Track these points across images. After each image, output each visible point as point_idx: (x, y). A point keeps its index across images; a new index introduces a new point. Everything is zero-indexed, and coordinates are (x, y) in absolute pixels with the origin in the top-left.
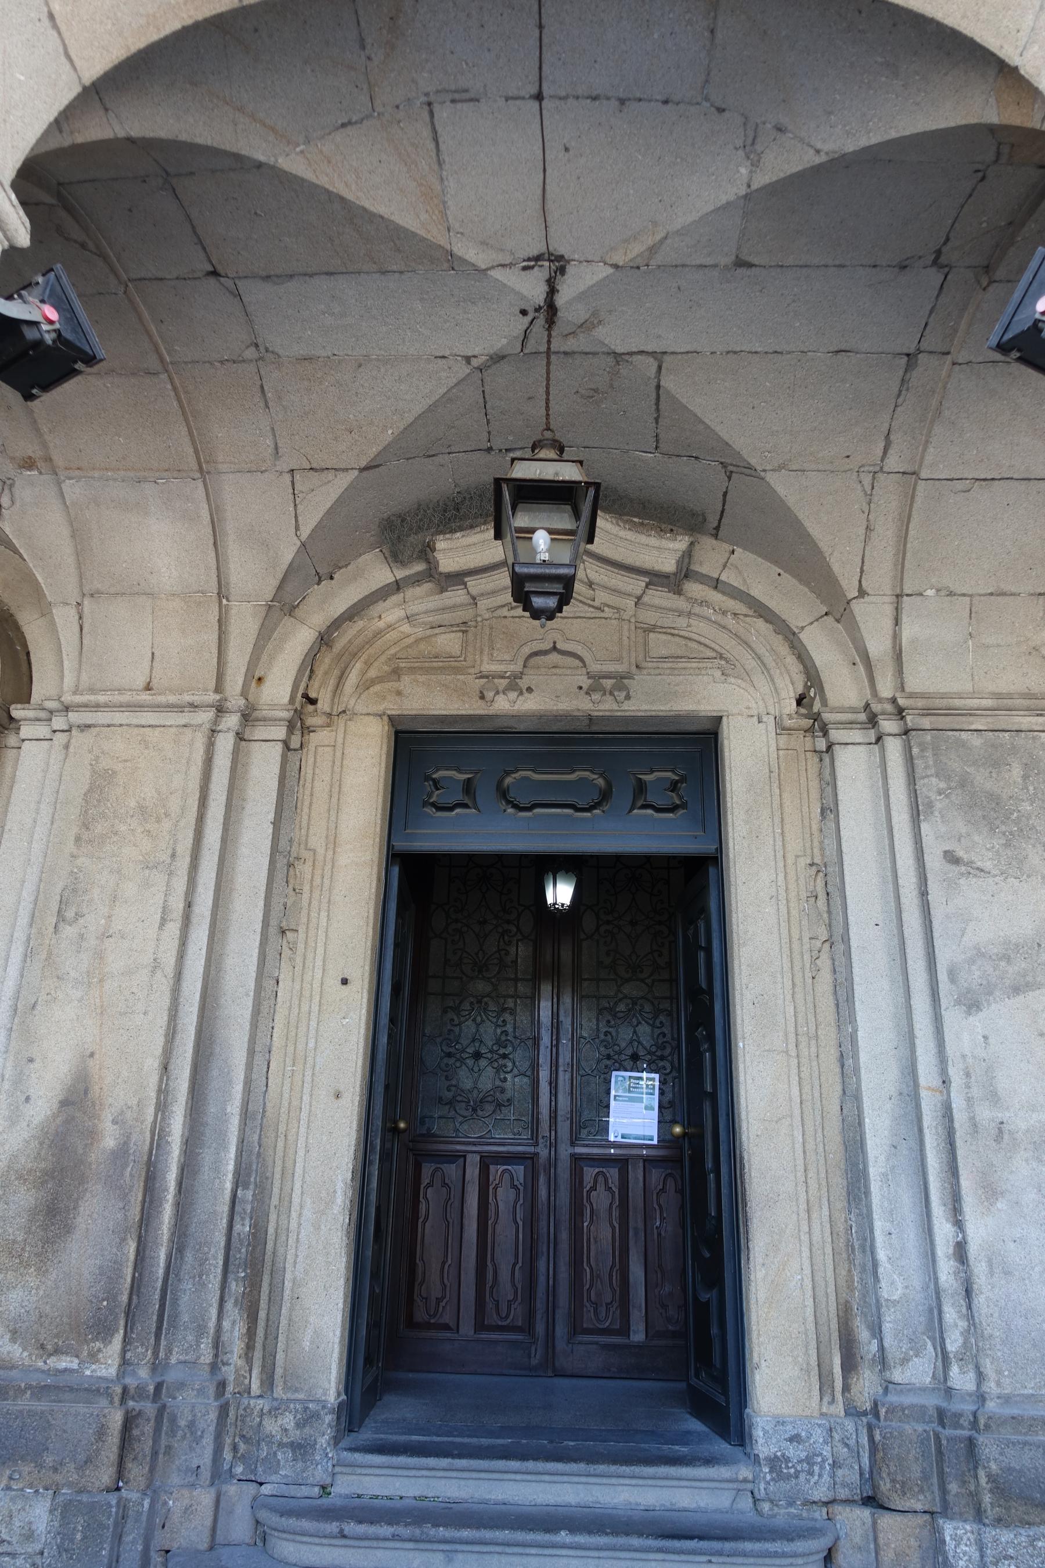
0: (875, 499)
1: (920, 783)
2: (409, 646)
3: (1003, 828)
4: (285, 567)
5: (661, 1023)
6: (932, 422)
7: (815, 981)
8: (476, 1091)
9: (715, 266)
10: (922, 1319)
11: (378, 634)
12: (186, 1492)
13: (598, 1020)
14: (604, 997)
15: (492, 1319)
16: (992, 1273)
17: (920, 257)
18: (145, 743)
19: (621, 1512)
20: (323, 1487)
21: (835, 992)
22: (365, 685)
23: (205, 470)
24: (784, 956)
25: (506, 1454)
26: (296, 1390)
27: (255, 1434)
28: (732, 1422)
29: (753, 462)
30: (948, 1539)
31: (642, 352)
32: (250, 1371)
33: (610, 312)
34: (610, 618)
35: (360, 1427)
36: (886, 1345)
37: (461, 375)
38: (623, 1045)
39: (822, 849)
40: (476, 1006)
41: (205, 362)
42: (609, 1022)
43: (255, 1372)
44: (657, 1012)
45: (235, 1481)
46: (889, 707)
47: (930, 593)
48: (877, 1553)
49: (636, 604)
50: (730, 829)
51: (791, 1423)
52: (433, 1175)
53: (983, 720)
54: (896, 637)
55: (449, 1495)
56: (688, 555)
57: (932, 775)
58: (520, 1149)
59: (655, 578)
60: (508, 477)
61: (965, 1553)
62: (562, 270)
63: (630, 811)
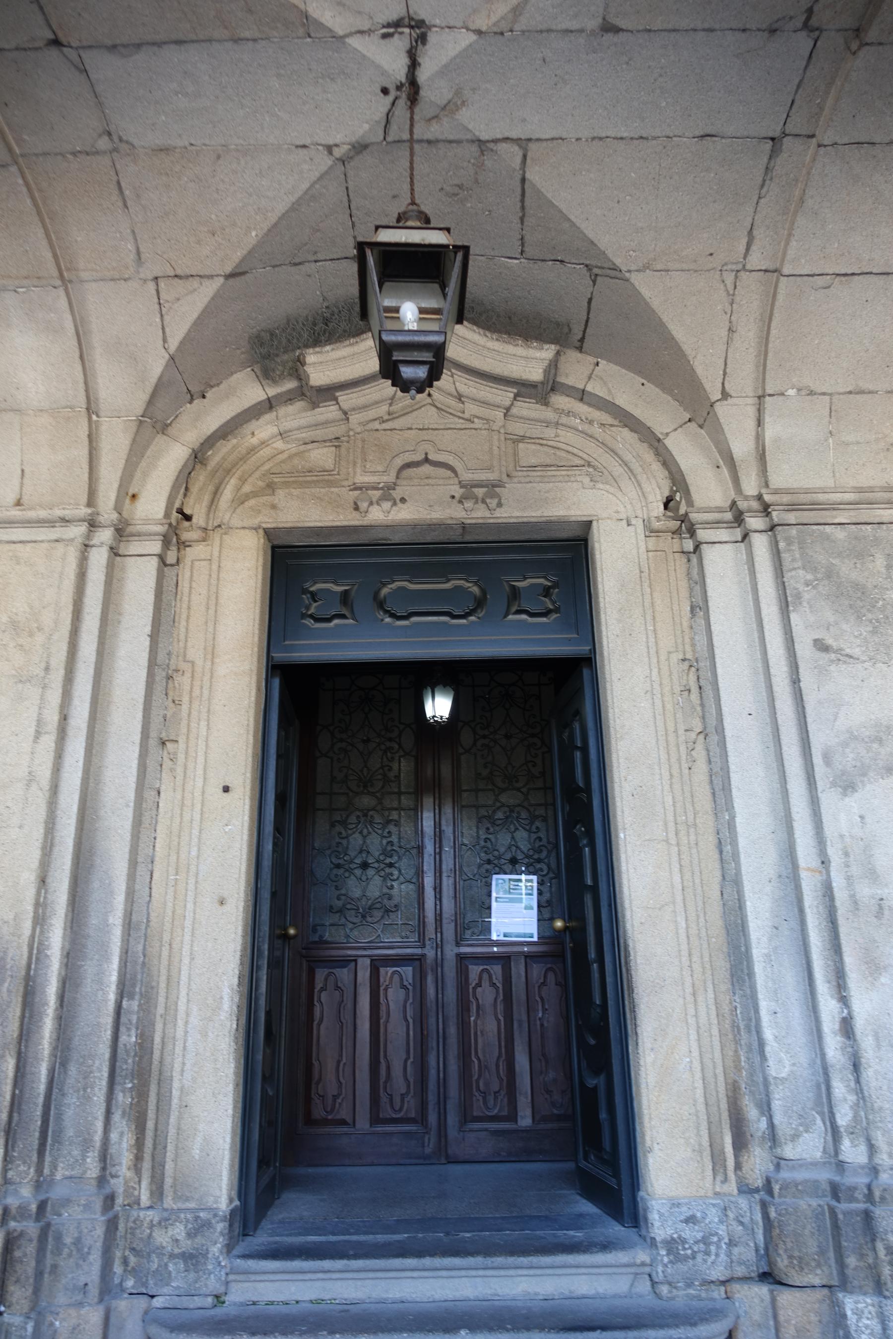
0: (737, 299)
1: (787, 576)
2: (283, 462)
3: (870, 616)
4: (154, 380)
5: (537, 828)
6: (796, 212)
7: (691, 771)
8: (364, 899)
9: (581, 31)
10: (810, 1095)
11: (252, 450)
12: (73, 1312)
13: (478, 828)
14: (483, 806)
15: (387, 1112)
16: (879, 1046)
17: (791, 18)
18: (17, 560)
19: (519, 1304)
20: (217, 1297)
21: (711, 782)
22: (240, 501)
23: (65, 278)
24: (661, 748)
25: (401, 1251)
26: (187, 1199)
27: (145, 1246)
28: (625, 1205)
29: (618, 261)
30: (849, 1313)
31: (506, 139)
32: (140, 1182)
33: (474, 90)
34: (480, 429)
35: (255, 1229)
36: (776, 1121)
37: (323, 168)
38: (502, 850)
39: (693, 645)
40: (362, 819)
41: (56, 154)
42: (488, 829)
43: (145, 1183)
44: (533, 818)
45: (126, 1295)
46: (755, 505)
47: (791, 392)
48: (777, 1330)
49: (505, 415)
50: (603, 628)
51: (687, 1204)
52: (326, 980)
53: (846, 514)
54: (759, 439)
55: (346, 1296)
56: (553, 366)
57: (799, 568)
58: (409, 951)
59: (524, 389)
60: (373, 240)
61: (867, 1327)
62: (423, 39)
63: (505, 617)
